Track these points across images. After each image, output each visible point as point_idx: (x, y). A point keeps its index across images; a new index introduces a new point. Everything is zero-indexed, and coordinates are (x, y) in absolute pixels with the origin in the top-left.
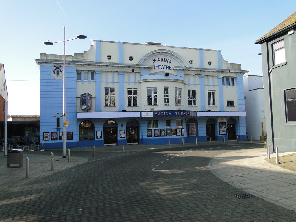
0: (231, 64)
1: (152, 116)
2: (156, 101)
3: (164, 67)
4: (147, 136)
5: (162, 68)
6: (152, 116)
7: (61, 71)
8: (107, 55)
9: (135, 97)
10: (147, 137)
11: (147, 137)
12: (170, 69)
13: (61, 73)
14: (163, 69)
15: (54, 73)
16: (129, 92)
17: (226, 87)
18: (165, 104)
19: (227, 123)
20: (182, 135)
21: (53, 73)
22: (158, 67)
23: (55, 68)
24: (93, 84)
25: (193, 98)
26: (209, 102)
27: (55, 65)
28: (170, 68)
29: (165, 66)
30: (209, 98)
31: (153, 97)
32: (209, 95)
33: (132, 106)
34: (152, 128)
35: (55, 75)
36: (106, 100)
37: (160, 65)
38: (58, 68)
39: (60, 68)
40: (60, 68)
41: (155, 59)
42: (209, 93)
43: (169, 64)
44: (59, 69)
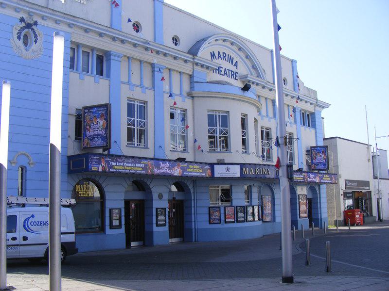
0: (307, 88)
1: (238, 175)
2: (226, 143)
3: (227, 71)
4: (208, 222)
5: (224, 74)
6: (238, 175)
7: (36, 36)
8: (287, 79)
9: (222, 132)
10: (210, 223)
11: (210, 223)
12: (236, 79)
13: (36, 41)
14: (225, 75)
15: (19, 38)
16: (211, 119)
17: (92, 79)
18: (76, 139)
19: (168, 210)
20: (238, 222)
21: (16, 36)
22: (219, 70)
23: (23, 25)
24: (103, 82)
25: (139, 124)
26: (130, 132)
27: (25, 16)
28: (236, 76)
29: (229, 70)
30: (130, 120)
31: (220, 134)
32: (130, 113)
33: (136, 147)
34: (219, 204)
35: (20, 43)
36: (263, 148)
37: (222, 68)
38: (29, 26)
39: (34, 27)
40: (34, 27)
41: (213, 52)
42: (130, 107)
43: (234, 69)
44: (33, 30)
